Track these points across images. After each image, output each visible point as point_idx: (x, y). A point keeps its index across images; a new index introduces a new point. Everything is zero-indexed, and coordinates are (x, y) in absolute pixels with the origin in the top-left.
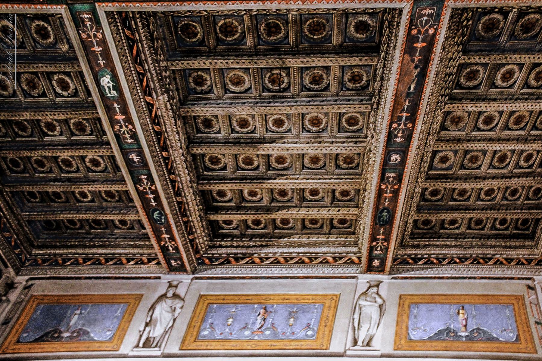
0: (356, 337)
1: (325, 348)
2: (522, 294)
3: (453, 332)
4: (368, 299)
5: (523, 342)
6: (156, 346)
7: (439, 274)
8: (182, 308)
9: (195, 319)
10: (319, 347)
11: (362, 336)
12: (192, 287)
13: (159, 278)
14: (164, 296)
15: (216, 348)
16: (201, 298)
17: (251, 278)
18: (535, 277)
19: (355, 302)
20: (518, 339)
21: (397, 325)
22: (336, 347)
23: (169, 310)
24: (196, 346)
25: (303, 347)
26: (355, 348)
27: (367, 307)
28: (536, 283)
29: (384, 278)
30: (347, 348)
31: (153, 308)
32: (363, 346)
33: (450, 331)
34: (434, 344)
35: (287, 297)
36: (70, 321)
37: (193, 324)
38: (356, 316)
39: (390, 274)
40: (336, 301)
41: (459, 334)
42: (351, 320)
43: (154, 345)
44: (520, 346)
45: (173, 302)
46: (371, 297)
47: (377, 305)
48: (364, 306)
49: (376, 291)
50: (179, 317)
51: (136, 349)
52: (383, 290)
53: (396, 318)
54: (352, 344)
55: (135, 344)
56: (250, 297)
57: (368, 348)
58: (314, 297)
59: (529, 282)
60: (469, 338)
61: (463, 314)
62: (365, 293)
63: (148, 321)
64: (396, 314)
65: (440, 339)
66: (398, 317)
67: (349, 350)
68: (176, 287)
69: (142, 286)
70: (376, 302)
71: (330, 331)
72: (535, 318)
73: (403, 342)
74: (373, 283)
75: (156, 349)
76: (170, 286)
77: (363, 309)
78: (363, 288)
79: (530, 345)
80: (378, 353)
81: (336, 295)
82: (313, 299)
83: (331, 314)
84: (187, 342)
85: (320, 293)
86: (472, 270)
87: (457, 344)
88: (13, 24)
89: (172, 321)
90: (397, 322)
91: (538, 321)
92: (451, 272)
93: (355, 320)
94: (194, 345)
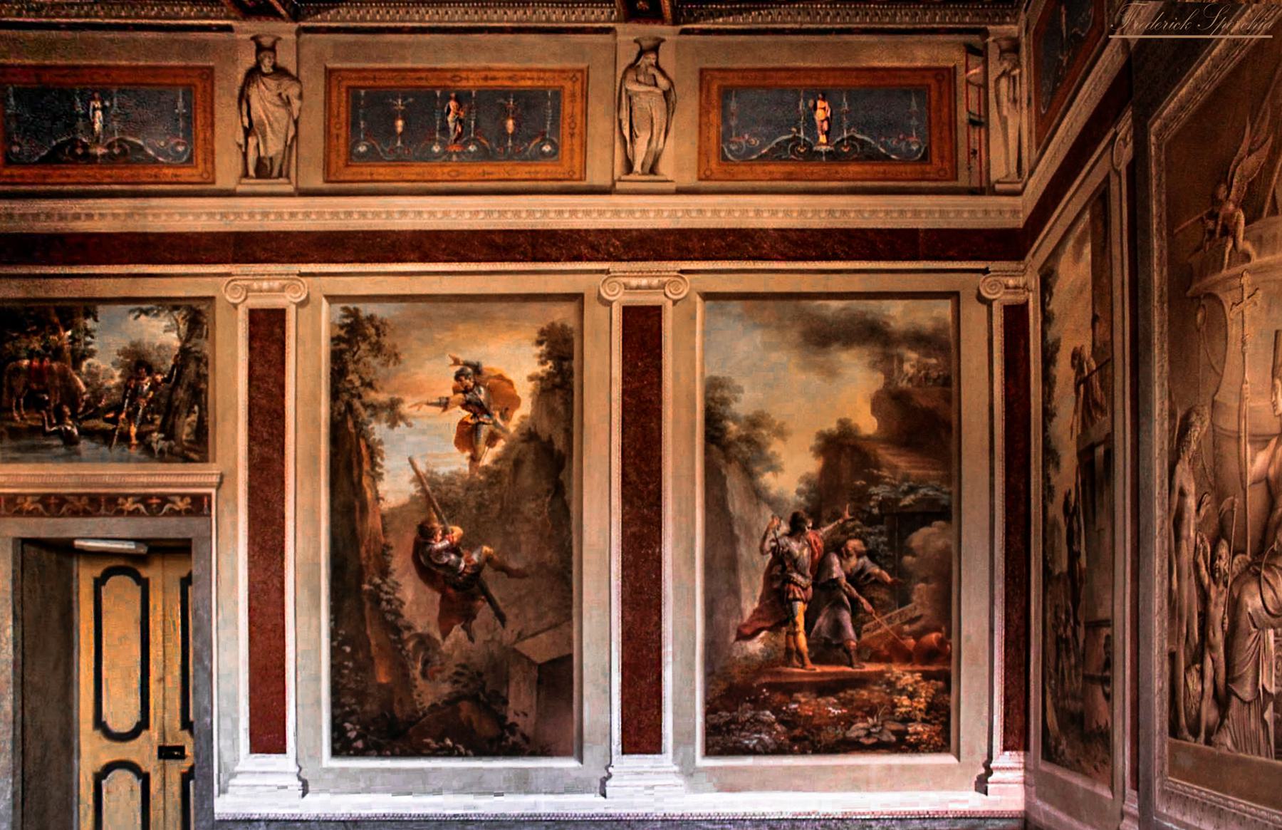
0: (630, 157)
1: (577, 176)
2: (952, 65)
3: (805, 145)
4: (641, 78)
5: (935, 160)
6: (280, 175)
7: (775, 22)
8: (300, 97)
9: (334, 121)
10: (567, 176)
11: (640, 152)
12: (304, 51)
13: (228, 29)
14: (254, 74)
15: (388, 178)
16: (330, 76)
17: (413, 31)
18: (990, 28)
19: (618, 88)
20: (926, 158)
21: (700, 133)
22: (597, 176)
23: (276, 100)
24: (354, 174)
25: (539, 176)
26: (631, 177)
27: (642, 96)
28: (990, 39)
29: (666, 31)
30: (616, 178)
31: (243, 97)
32: (644, 174)
33: (798, 144)
34: (768, 168)
35: (490, 74)
36: (93, 124)
37: (334, 131)
38: (624, 114)
39: (675, 22)
40: (582, 83)
41: (815, 148)
42: (617, 124)
43: (275, 172)
44: (928, 168)
45: (279, 85)
46: (646, 73)
47: (658, 91)
48: (637, 94)
49: (653, 62)
50: (303, 114)
51: (244, 181)
52: (667, 58)
53: (697, 118)
54: (624, 170)
55: (240, 169)
56: (423, 75)
57: (652, 177)
58: (542, 75)
59: (974, 39)
60: (833, 156)
61: (824, 109)
62: (633, 67)
63: (246, 124)
64: (697, 112)
65: (779, 158)
66: (700, 115)
67: (620, 180)
68: (272, 49)
69: (203, 48)
70: (656, 85)
71: (582, 145)
72: (970, 113)
73: (714, 164)
74: (647, 44)
75: (281, 180)
76: (260, 49)
77: (635, 100)
78: (627, 56)
79: (947, 165)
80: (672, 187)
81: (581, 71)
82: (539, 79)
83: (578, 110)
84: (333, 170)
85: (549, 66)
86: (843, 13)
87: (809, 168)
88: (1240, 32)
89: (292, 128)
90: (700, 127)
91: (976, 119)
92: (799, 19)
93: (624, 122)
94: (348, 174)
